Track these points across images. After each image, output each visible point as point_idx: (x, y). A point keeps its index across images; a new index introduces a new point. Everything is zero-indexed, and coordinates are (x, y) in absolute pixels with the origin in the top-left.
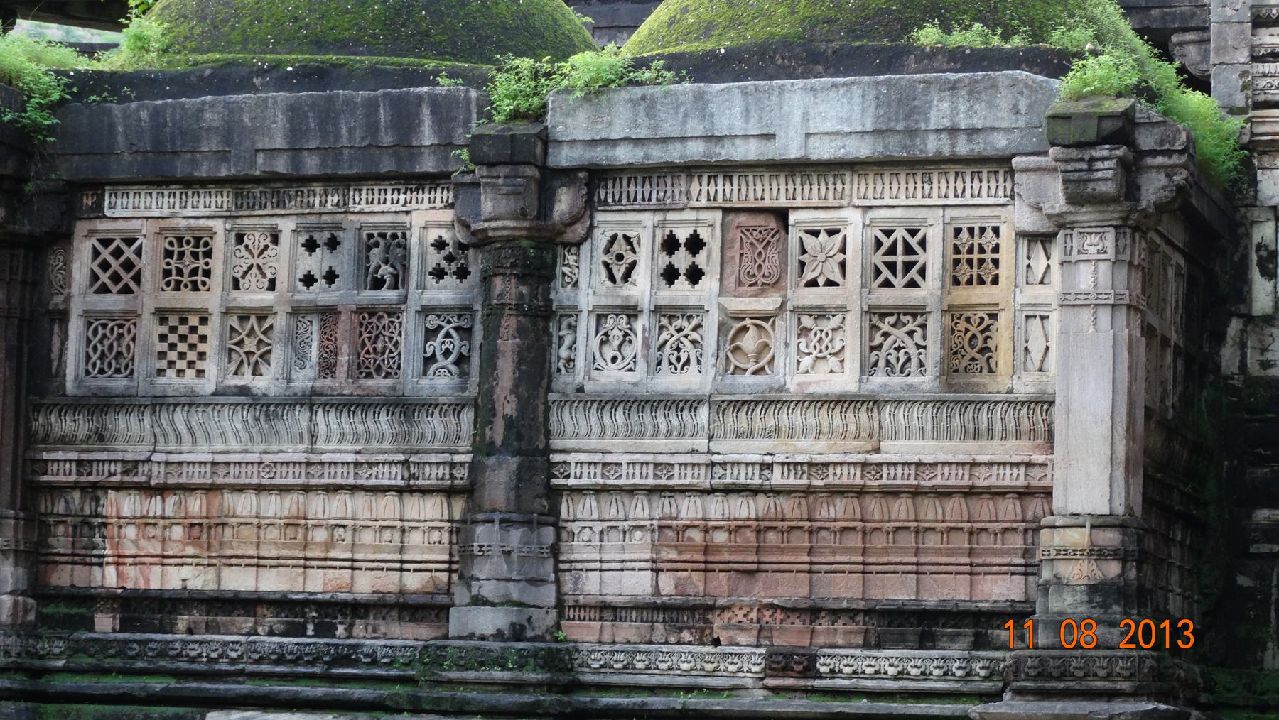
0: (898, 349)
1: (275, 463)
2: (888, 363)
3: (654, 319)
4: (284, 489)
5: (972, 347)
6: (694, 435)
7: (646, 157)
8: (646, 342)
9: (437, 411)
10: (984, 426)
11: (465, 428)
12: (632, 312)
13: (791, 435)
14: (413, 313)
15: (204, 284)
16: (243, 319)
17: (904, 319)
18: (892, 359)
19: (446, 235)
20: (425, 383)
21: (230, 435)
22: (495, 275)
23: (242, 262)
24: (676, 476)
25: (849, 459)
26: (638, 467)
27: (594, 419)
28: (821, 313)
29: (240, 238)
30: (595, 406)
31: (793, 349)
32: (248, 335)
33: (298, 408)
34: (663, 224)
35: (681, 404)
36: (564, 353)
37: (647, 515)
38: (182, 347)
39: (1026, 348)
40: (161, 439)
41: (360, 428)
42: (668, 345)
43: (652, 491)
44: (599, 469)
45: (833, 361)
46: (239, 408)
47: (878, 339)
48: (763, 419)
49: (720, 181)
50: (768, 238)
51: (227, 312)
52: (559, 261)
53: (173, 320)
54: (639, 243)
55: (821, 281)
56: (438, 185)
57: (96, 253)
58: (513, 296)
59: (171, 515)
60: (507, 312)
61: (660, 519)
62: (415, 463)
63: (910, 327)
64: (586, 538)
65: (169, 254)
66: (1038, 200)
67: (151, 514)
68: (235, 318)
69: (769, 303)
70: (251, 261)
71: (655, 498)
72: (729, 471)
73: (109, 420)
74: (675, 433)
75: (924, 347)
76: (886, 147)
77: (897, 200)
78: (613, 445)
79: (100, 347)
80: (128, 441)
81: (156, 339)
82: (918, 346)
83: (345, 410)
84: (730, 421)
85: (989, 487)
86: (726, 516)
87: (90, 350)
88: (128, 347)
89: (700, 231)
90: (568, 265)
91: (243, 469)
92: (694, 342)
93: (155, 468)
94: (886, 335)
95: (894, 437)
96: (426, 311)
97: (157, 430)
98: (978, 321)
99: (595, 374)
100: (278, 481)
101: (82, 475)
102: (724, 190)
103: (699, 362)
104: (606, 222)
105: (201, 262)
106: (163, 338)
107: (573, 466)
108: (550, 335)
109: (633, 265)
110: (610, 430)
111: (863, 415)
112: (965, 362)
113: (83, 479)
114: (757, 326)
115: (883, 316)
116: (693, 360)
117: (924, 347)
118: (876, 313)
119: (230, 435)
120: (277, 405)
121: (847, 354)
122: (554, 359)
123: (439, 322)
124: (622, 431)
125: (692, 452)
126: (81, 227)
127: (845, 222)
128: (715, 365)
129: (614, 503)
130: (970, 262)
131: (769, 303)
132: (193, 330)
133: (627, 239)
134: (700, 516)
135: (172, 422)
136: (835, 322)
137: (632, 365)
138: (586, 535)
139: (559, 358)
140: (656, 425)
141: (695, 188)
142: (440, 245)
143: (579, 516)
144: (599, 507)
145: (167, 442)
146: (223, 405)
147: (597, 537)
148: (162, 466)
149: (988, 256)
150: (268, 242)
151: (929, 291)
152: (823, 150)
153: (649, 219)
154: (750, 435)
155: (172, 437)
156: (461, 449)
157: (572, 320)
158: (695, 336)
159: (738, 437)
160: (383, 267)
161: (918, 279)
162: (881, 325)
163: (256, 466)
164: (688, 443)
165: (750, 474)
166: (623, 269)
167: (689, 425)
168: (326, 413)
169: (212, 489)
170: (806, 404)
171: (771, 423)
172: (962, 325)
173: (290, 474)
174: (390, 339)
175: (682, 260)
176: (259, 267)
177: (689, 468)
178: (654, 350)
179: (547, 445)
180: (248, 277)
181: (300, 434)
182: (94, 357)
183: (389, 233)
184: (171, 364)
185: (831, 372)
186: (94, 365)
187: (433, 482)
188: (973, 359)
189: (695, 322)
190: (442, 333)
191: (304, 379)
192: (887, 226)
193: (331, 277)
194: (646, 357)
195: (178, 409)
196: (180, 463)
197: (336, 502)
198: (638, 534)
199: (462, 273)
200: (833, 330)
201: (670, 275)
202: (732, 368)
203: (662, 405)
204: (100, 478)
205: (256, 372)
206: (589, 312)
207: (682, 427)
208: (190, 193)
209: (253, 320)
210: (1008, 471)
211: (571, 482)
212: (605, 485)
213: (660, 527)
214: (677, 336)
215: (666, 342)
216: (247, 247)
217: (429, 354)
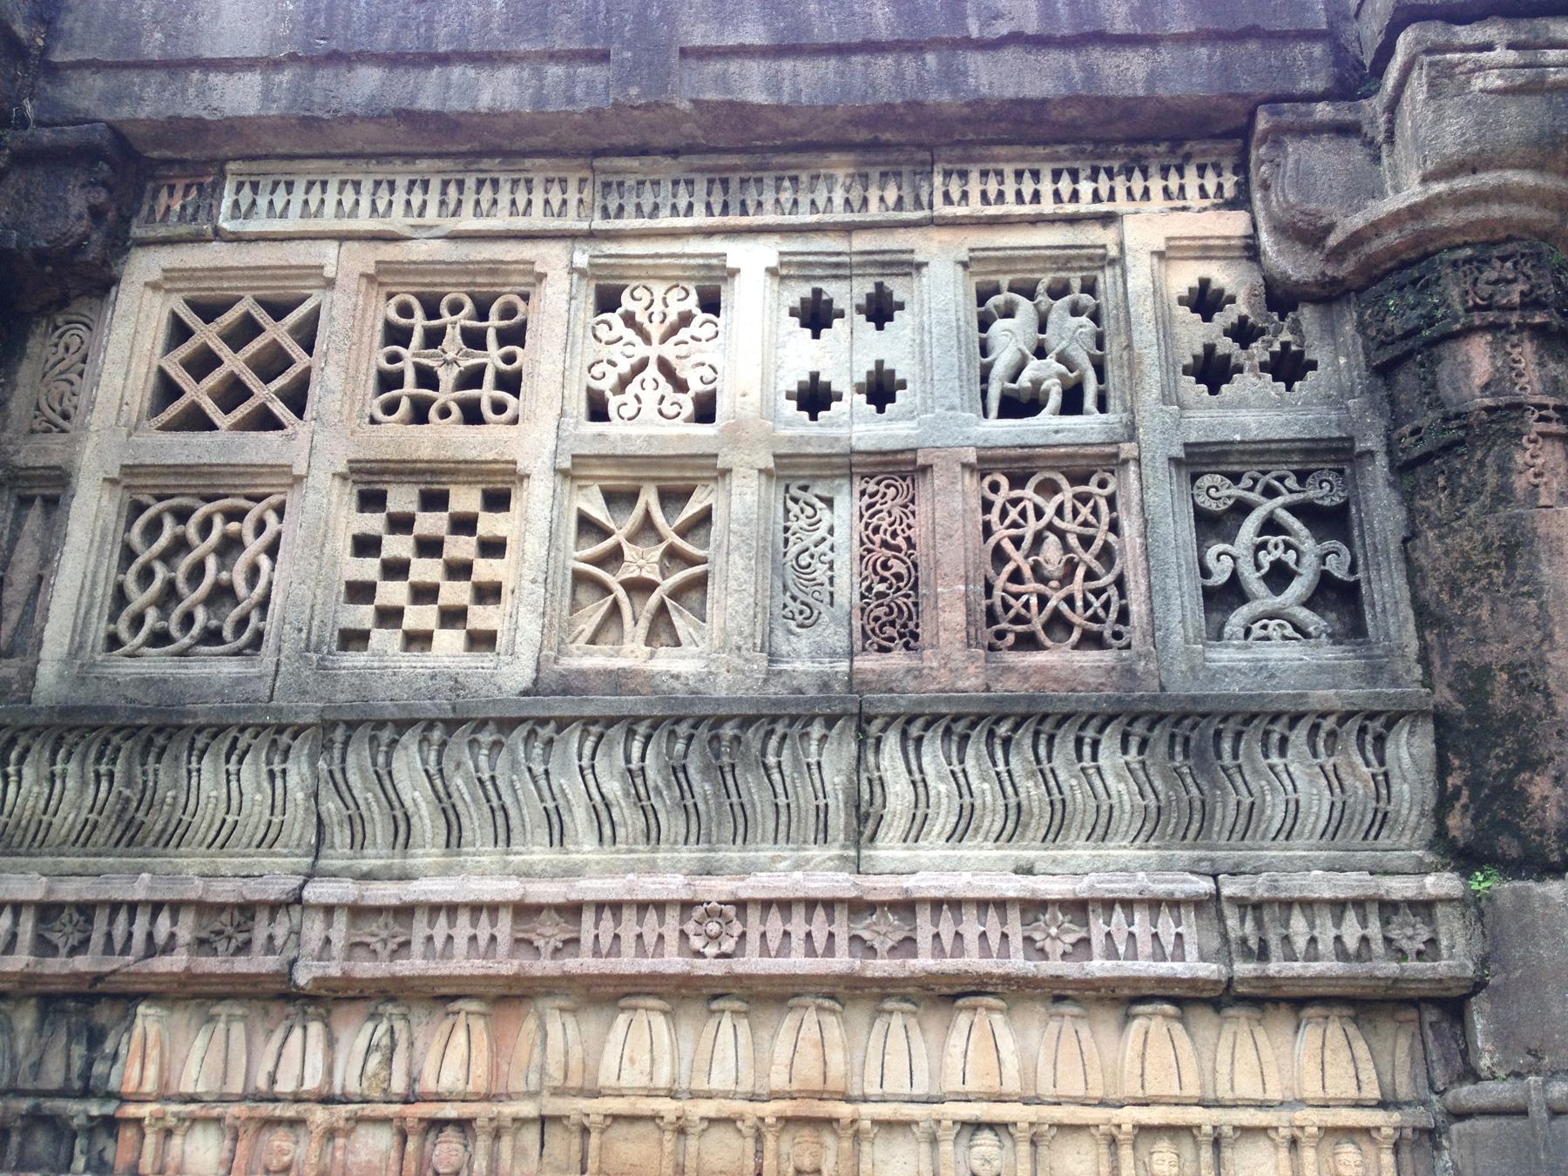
1: (741, 905)
4: (770, 996)
9: (1299, 736)
11: (1402, 789)
14: (1161, 463)
15: (499, 407)
16: (619, 498)
19: (1222, 276)
20: (1223, 656)
21: (579, 819)
22: (1469, 331)
23: (615, 352)
29: (607, 301)
32: (632, 539)
33: (816, 730)
38: (426, 570)
40: (339, 836)
44: (505, 926)
46: (617, 732)
51: (572, 473)
53: (402, 499)
56: (1188, 157)
57: (179, 332)
59: (353, 1087)
62: (1241, 903)
65: (397, 335)
67: (285, 1085)
70: (640, 350)
73: (164, 777)
79: (161, 572)
80: (222, 840)
81: (344, 545)
87: (130, 579)
88: (254, 571)
91: (629, 926)
96: (1196, 460)
97: (331, 805)
100: (752, 963)
101: (53, 950)
105: (493, 357)
106: (365, 546)
113: (55, 965)
120: (746, 722)
123: (1236, 492)
132: (464, 525)
135: (384, 778)
142: (1205, 301)
145: (358, 842)
146: (563, 724)
148: (341, 920)
150: (692, 303)
155: (379, 829)
156: (1394, 859)
163: (672, 917)
168: (911, 745)
169: (509, 997)
173: (797, 941)
174: (1086, 542)
176: (665, 367)
180: (633, 388)
181: (822, 813)
182: (139, 599)
183: (1046, 280)
186: (138, 621)
187: (1328, 966)
192: (210, 290)
193: (881, 389)
196: (405, 911)
197: (957, 1040)
204: (115, 963)
205: (661, 628)
208: (470, 182)
209: (649, 498)
210: (798, 926)
216: (629, 320)
217: (1220, 577)
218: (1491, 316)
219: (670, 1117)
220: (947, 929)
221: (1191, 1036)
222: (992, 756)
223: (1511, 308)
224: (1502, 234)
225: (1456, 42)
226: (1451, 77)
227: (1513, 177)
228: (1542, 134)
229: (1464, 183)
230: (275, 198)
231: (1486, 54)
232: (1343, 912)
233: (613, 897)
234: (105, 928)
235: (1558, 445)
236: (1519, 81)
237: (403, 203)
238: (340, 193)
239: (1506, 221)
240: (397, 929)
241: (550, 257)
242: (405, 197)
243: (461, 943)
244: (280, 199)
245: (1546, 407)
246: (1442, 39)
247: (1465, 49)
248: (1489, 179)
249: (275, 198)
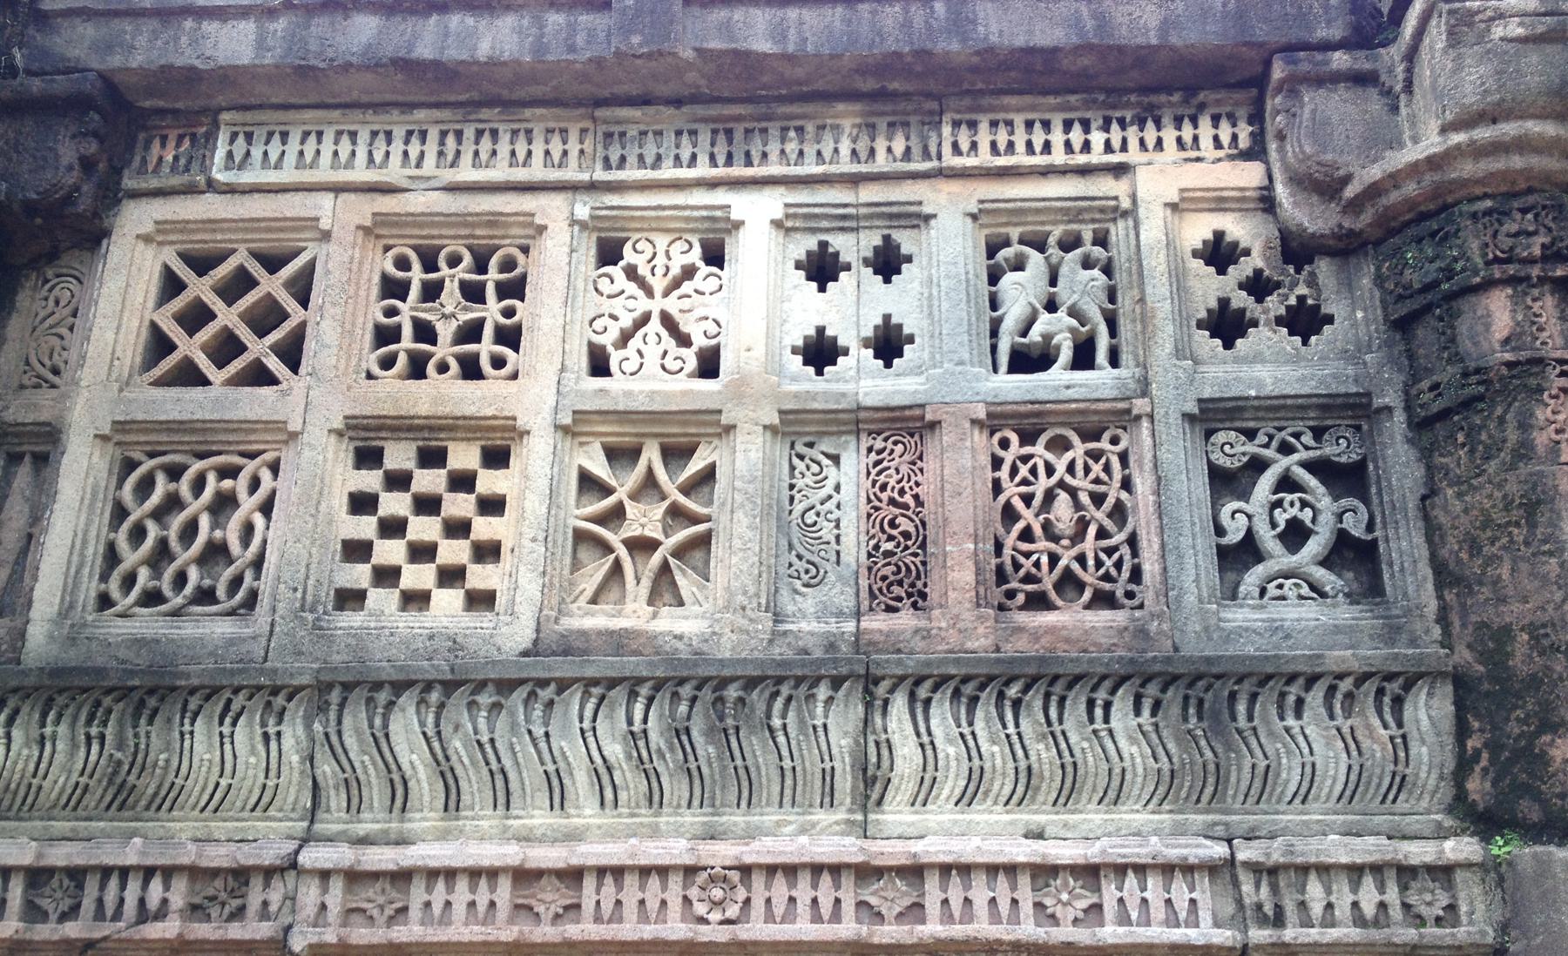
1: (746, 870)
9: (1315, 698)
14: (1175, 419)
15: (498, 362)
16: (620, 455)
19: (1237, 228)
20: (1239, 616)
21: (581, 783)
22: (1489, 284)
23: (617, 306)
29: (609, 254)
32: (634, 496)
33: (823, 692)
38: (424, 528)
40: (335, 800)
41: (1042, 753)
46: (619, 694)
53: (399, 456)
56: (1202, 107)
57: (172, 285)
62: (1256, 869)
65: (394, 289)
68: (596, 450)
70: (643, 304)
73: (156, 739)
80: (215, 804)
81: (340, 503)
83: (988, 697)
88: (248, 530)
91: (631, 891)
93: (310, 894)
96: (1210, 417)
97: (326, 768)
101: (44, 916)
105: (492, 311)
119: (581, 783)
120: (751, 683)
123: (1251, 448)
126: (136, 218)
132: (462, 482)
135: (381, 741)
145: (354, 806)
146: (563, 685)
148: (337, 886)
155: (376, 792)
156: (1413, 823)
160: (1044, 317)
163: (675, 882)
168: (920, 706)
173: (803, 907)
174: (1098, 499)
176: (668, 321)
181: (828, 776)
182: (131, 557)
183: (1057, 232)
184: (387, 576)
186: (129, 581)
190: (1267, 481)
191: (817, 616)
193: (888, 344)
195: (408, 701)
199: (1304, 322)
204: (106, 929)
205: (664, 587)
209: (651, 454)
210: (803, 892)
216: (631, 273)
217: (1234, 536)
218: (1511, 269)
223: (1531, 261)
226: (1471, 25)
227: (1534, 127)
229: (1483, 133)
234: (96, 894)
236: (1540, 29)
239: (1527, 173)
240: (394, 894)
248: (1509, 129)
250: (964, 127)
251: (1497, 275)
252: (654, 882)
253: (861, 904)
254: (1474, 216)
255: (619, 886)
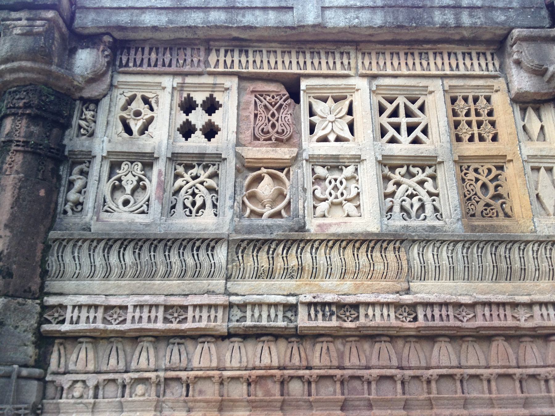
0: (411, 196)
2: (403, 209)
3: (171, 167)
5: (485, 194)
6: (211, 275)
7: (170, 22)
8: (162, 186)
10: (517, 266)
12: (148, 161)
13: (314, 275)
17: (414, 170)
18: (407, 205)
24: (190, 319)
25: (383, 298)
26: (146, 310)
27: (99, 260)
28: (335, 164)
30: (102, 245)
31: (309, 194)
34: (181, 87)
35: (198, 244)
36: (73, 196)
37: (152, 366)
39: (537, 195)
42: (183, 191)
43: (161, 338)
44: (100, 313)
45: (349, 207)
47: (391, 187)
48: (285, 259)
49: (236, 54)
50: (281, 102)
52: (76, 114)
54: (157, 102)
55: (332, 137)
58: (22, 134)
60: (14, 148)
61: (166, 370)
63: (421, 176)
64: (77, 394)
66: (541, 63)
69: (284, 153)
71: (162, 345)
72: (249, 313)
74: (189, 273)
75: (437, 195)
76: (396, 18)
77: (399, 73)
78: (119, 287)
82: (430, 194)
84: (249, 262)
85: (534, 329)
86: (244, 364)
89: (215, 95)
90: (85, 120)
91: (84, 313)
92: (211, 190)
94: (398, 184)
95: (423, 277)
98: (486, 172)
99: (104, 216)
102: (242, 63)
103: (215, 206)
104: (126, 83)
107: (70, 309)
108: (59, 178)
109: (151, 120)
110: (116, 271)
111: (391, 255)
112: (480, 207)
114: (271, 175)
115: (393, 168)
116: (209, 204)
117: (437, 195)
118: (388, 164)
121: (364, 200)
122: (61, 200)
124: (130, 272)
125: (209, 292)
127: (354, 89)
128: (232, 207)
129: (114, 353)
130: (469, 124)
131: (284, 153)
133: (146, 101)
134: (214, 364)
136: (348, 171)
137: (145, 208)
138: (78, 390)
139: (66, 201)
140: (169, 265)
141: (212, 58)
143: (71, 367)
144: (96, 358)
147: (91, 393)
149: (484, 117)
151: (438, 142)
152: (337, 20)
153: (168, 82)
154: (270, 274)
157: (83, 166)
158: (211, 182)
159: (258, 277)
161: (422, 136)
162: (392, 175)
164: (204, 284)
165: (273, 316)
166: (140, 123)
167: (206, 264)
170: (330, 244)
171: (293, 262)
172: (472, 175)
175: (198, 118)
177: (205, 310)
178: (168, 194)
179: (42, 287)
185: (348, 216)
188: (487, 205)
189: (211, 170)
192: (390, 93)
194: (160, 199)
198: (140, 389)
200: (347, 179)
201: (187, 131)
202: (248, 211)
203: (177, 245)
206: (103, 158)
207: (198, 266)
211: (66, 327)
212: (105, 331)
213: (166, 379)
214: (192, 182)
215: (181, 188)
218: (13, 111)
219: (278, 376)
220: (92, 315)
221: (277, 348)
222: (339, 253)
223: (19, 108)
224: (28, 83)
225: (10, 17)
226: (9, 29)
227: (24, 63)
228: (30, 50)
229: (9, 65)
230: (227, 59)
231: (19, 22)
232: (261, 308)
233: (545, 301)
234: (267, 314)
235: (21, 154)
236: (25, 31)
237: (310, 63)
238: (225, 56)
239: (24, 79)
240: (353, 312)
241: (436, 85)
242: (478, 62)
243: (437, 316)
244: (139, 57)
245: (20, 141)
246: (5, 17)
247: (14, 20)
248: (16, 64)
249: (227, 59)
250: (301, 53)
251: (8, 112)
252: (92, 310)
253: (513, 316)
254: (10, 93)
255: (201, 311)
